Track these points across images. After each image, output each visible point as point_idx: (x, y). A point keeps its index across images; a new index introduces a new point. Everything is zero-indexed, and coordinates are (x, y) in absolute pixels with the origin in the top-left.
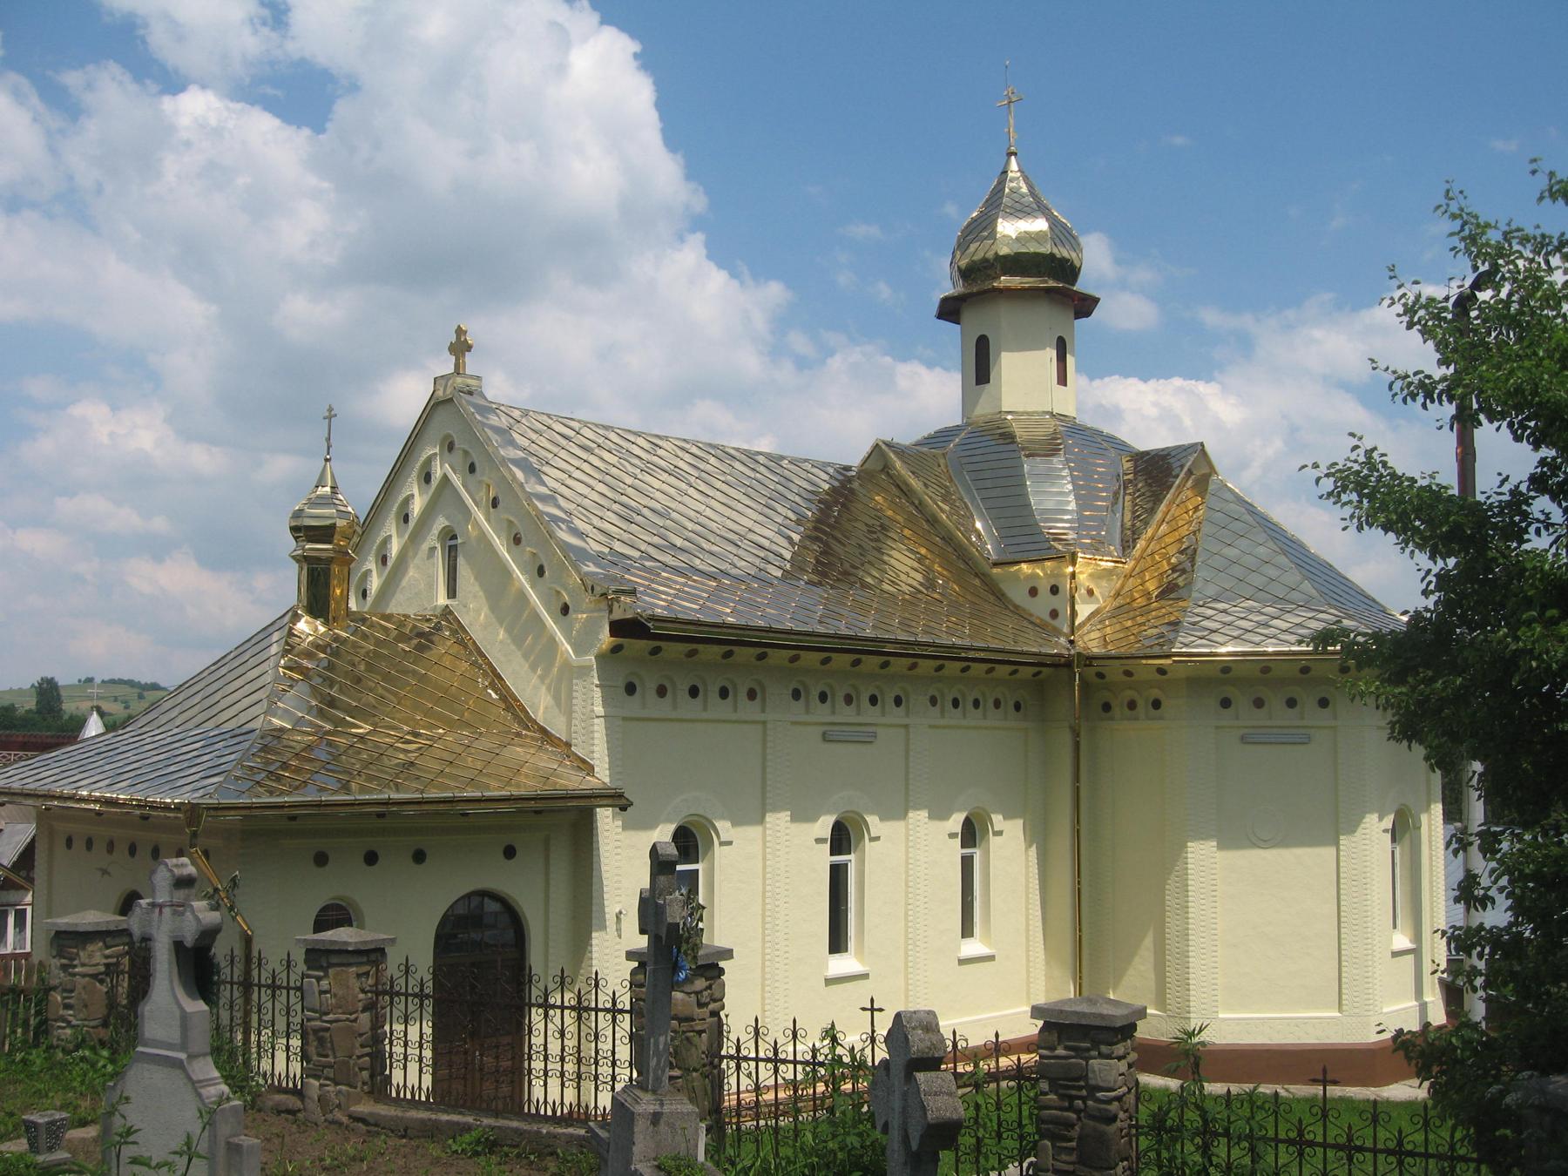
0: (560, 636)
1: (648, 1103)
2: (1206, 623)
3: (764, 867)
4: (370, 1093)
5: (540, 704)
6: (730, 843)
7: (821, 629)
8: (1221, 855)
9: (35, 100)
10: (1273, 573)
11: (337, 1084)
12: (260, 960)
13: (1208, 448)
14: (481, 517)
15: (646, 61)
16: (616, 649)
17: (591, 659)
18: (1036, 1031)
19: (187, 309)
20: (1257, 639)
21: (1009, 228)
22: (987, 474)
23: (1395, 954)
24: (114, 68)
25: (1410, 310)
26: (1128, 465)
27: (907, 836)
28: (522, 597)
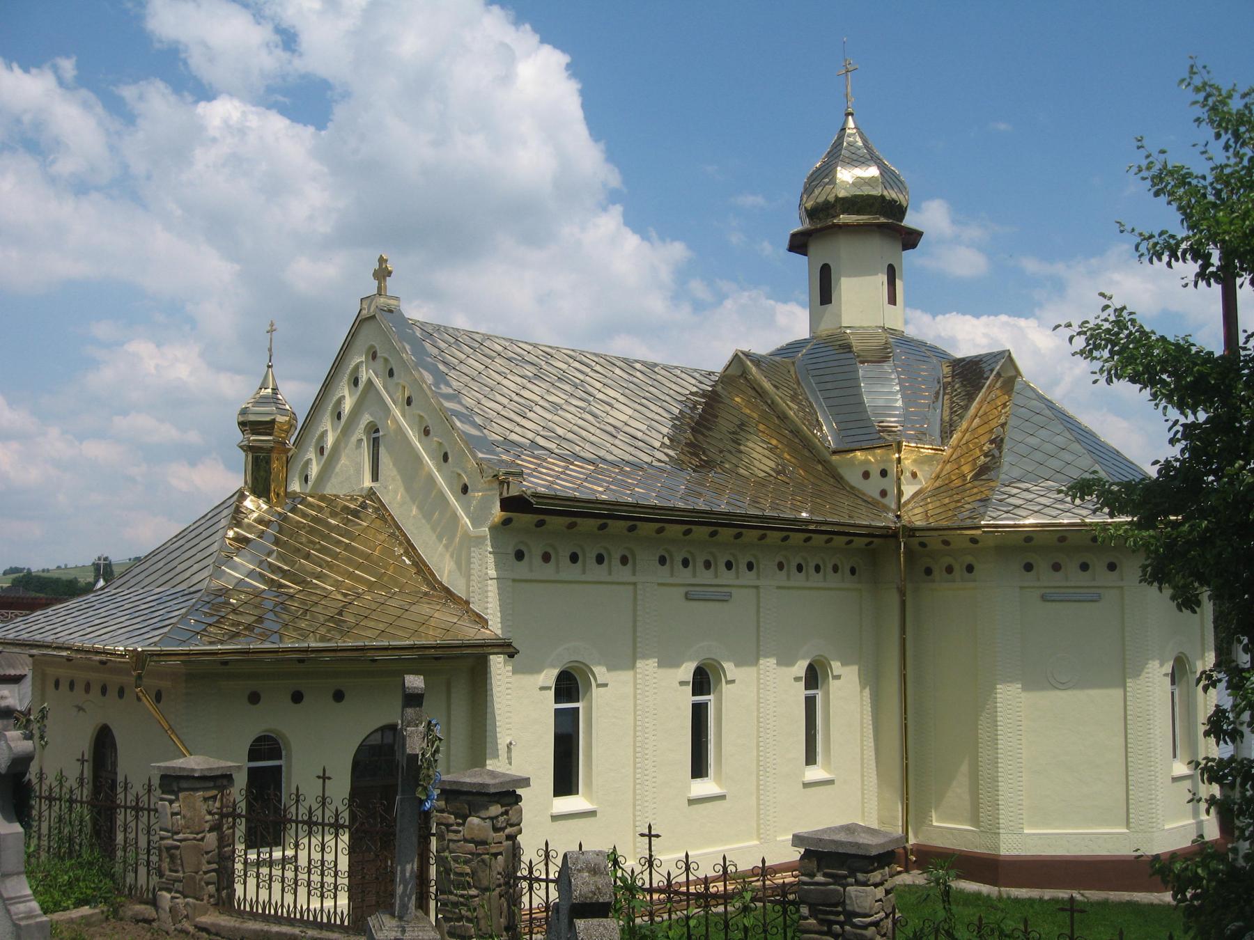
0: (460, 512)
1: (391, 929)
2: (1011, 500)
3: (635, 705)
4: (216, 905)
5: (446, 571)
6: (606, 685)
7: (681, 505)
8: (1023, 695)
9: (99, 109)
10: (1068, 457)
11: (185, 897)
12: (126, 784)
13: (1014, 356)
14: (397, 413)
15: (574, 70)
16: (506, 522)
17: (485, 530)
18: (798, 857)
19: (213, 268)
20: (1055, 513)
21: (846, 176)
22: (827, 378)
23: (1175, 779)
24: (161, 85)
25: (1158, 178)
26: (947, 370)
27: (759, 679)
28: (431, 479)
